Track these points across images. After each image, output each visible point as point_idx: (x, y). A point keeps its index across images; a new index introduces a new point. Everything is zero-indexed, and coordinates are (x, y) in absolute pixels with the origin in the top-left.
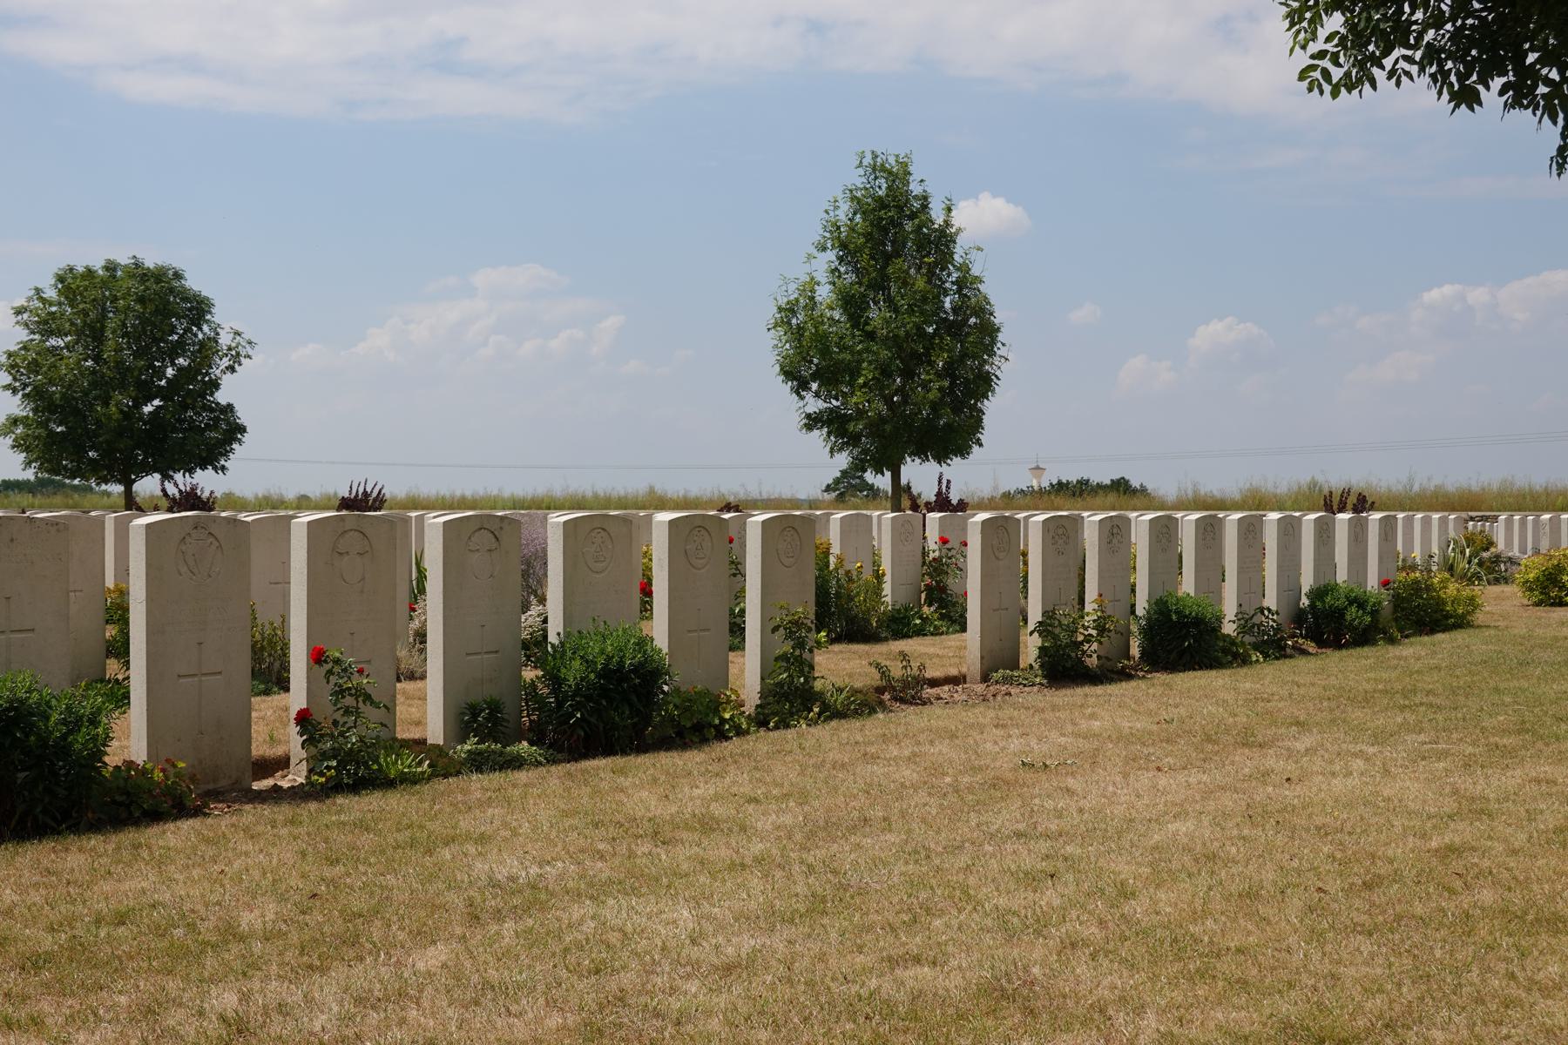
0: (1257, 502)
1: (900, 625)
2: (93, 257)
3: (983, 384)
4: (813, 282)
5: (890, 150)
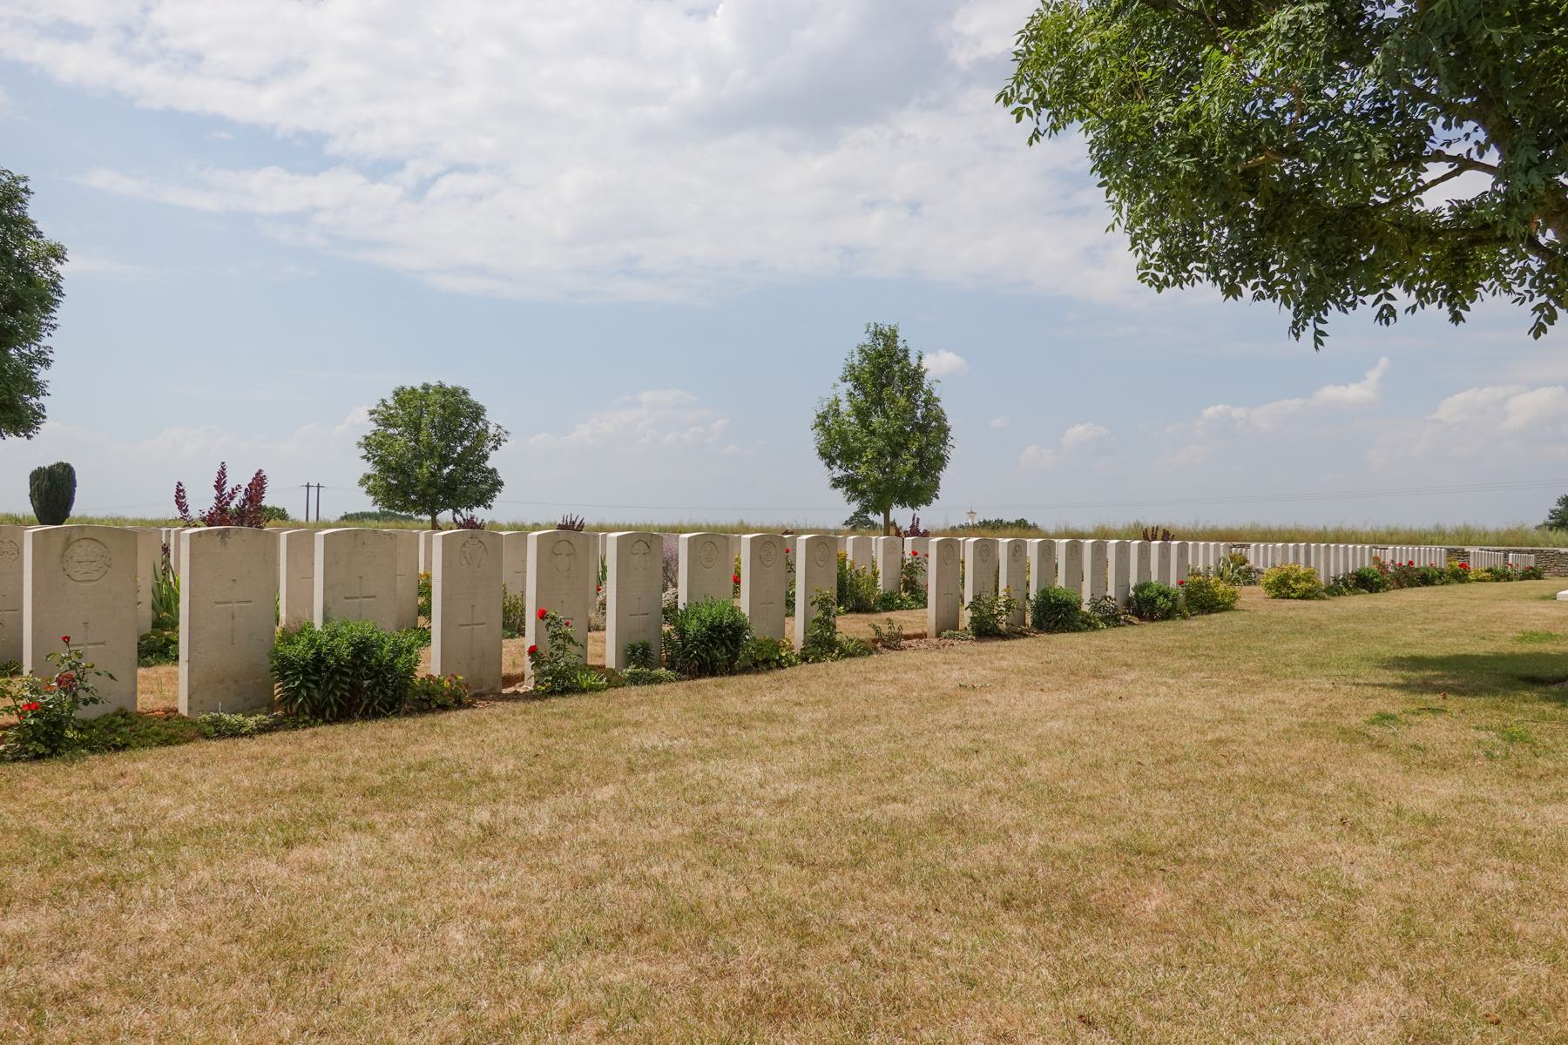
0: (1102, 535)
1: (888, 603)
2: (415, 381)
3: (941, 461)
4: (837, 401)
5: (886, 323)
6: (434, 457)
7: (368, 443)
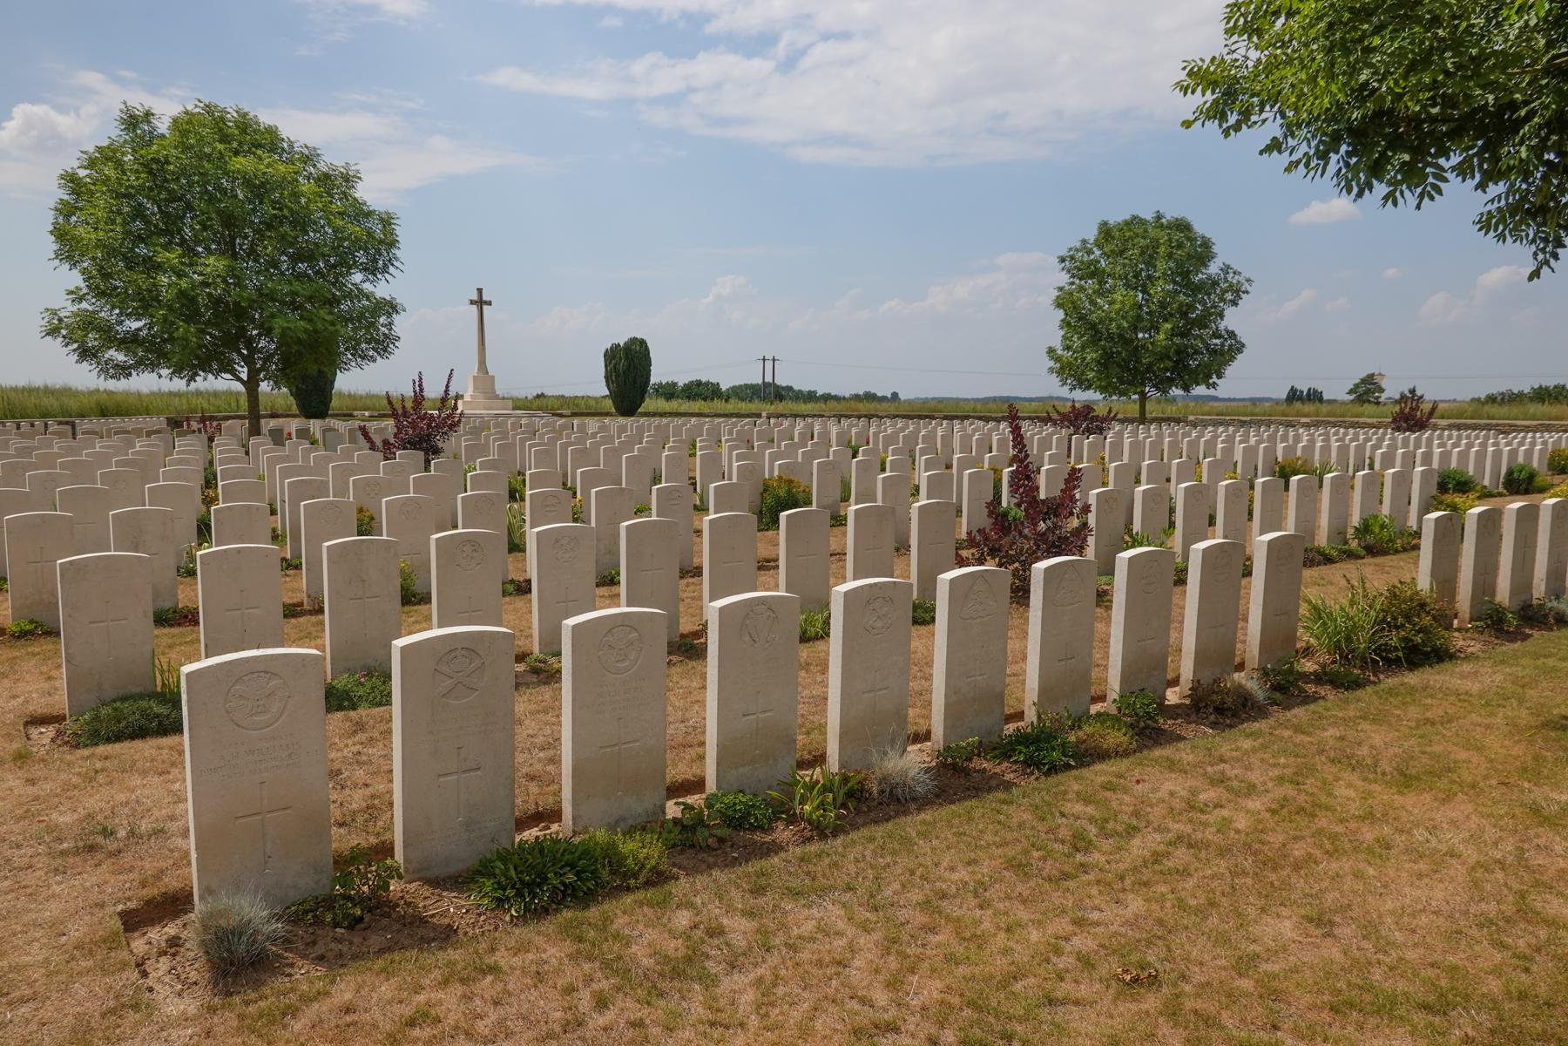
3: (46, 387)
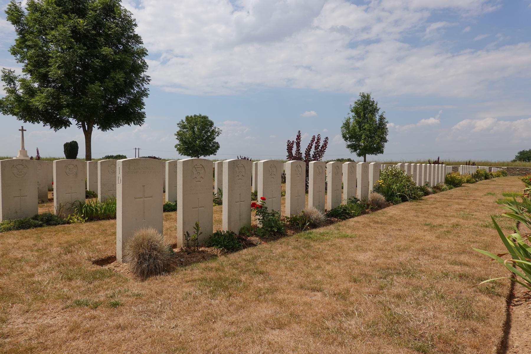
0: (411, 163)
2: (191, 114)
6: (366, 129)
7: (178, 134)
